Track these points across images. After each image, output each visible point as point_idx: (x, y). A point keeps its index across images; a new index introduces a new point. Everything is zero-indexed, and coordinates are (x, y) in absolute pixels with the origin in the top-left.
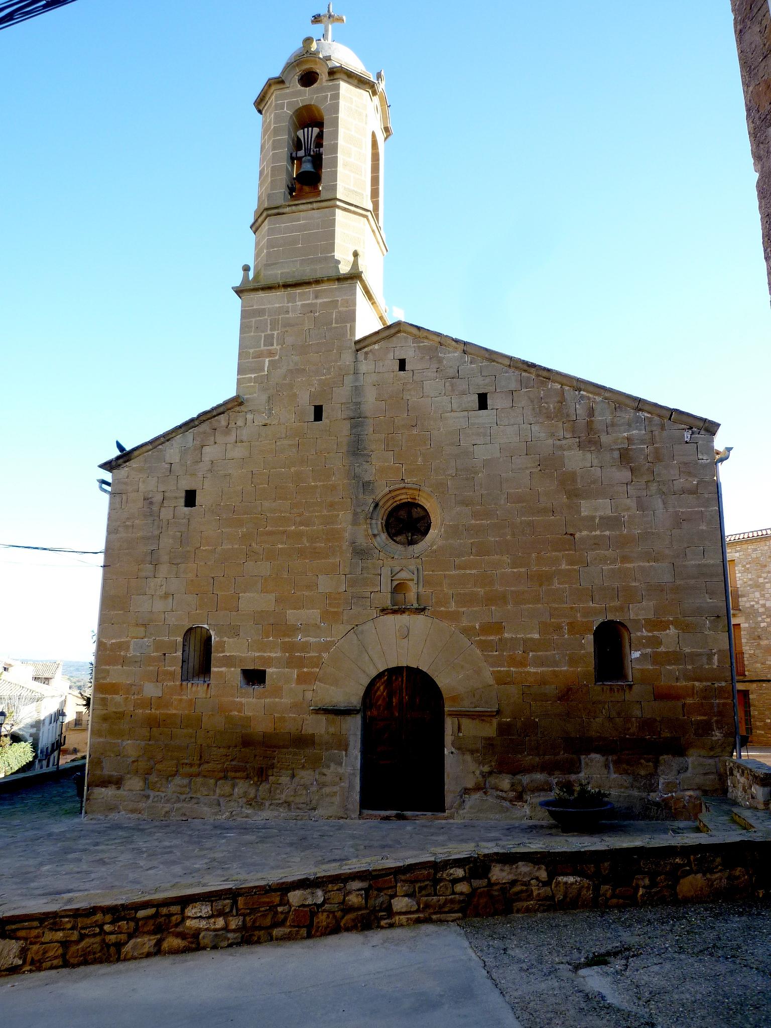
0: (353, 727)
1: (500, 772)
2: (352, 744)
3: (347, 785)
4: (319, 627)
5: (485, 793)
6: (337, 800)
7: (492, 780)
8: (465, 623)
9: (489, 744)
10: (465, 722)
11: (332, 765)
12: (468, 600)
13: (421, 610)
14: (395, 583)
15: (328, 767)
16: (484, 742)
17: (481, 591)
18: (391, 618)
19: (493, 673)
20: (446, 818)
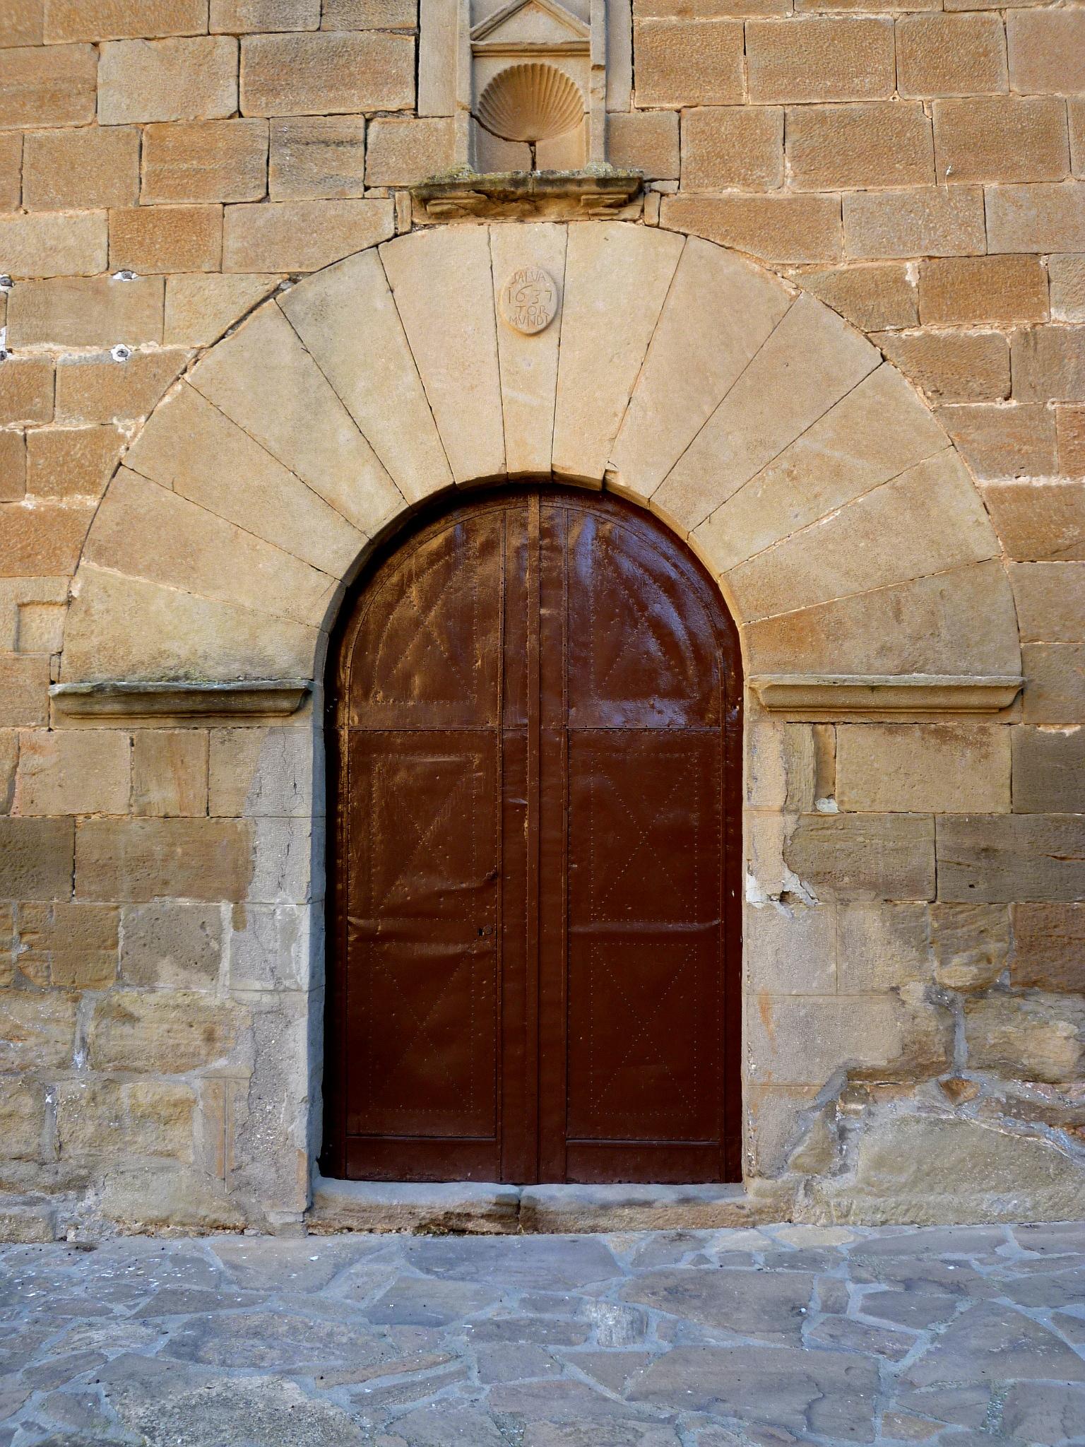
0: (277, 776)
1: (1030, 986)
2: (265, 862)
3: (242, 1067)
4: (100, 291)
5: (951, 1090)
6: (194, 1137)
7: (991, 1027)
8: (847, 255)
9: (974, 852)
10: (854, 745)
11: (169, 976)
12: (865, 147)
13: (624, 194)
14: (494, 68)
15: (147, 980)
16: (943, 838)
17: (927, 105)
18: (469, 239)
19: (992, 501)
20: (751, 1219)
